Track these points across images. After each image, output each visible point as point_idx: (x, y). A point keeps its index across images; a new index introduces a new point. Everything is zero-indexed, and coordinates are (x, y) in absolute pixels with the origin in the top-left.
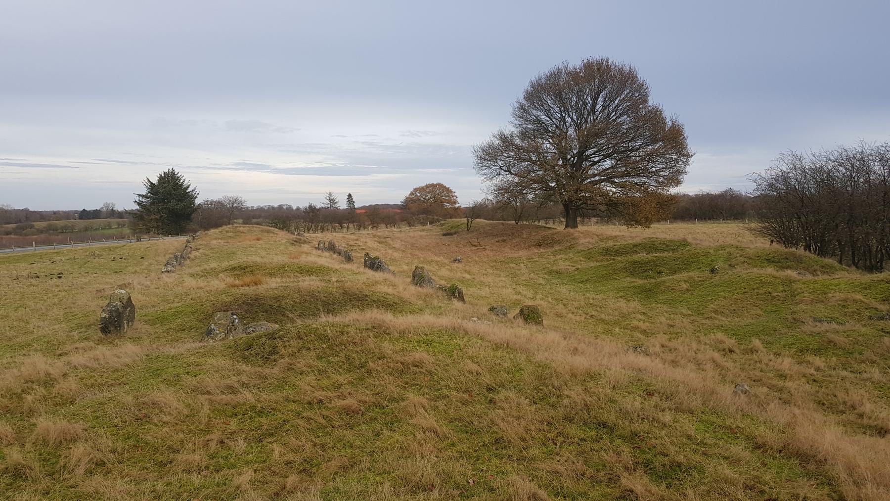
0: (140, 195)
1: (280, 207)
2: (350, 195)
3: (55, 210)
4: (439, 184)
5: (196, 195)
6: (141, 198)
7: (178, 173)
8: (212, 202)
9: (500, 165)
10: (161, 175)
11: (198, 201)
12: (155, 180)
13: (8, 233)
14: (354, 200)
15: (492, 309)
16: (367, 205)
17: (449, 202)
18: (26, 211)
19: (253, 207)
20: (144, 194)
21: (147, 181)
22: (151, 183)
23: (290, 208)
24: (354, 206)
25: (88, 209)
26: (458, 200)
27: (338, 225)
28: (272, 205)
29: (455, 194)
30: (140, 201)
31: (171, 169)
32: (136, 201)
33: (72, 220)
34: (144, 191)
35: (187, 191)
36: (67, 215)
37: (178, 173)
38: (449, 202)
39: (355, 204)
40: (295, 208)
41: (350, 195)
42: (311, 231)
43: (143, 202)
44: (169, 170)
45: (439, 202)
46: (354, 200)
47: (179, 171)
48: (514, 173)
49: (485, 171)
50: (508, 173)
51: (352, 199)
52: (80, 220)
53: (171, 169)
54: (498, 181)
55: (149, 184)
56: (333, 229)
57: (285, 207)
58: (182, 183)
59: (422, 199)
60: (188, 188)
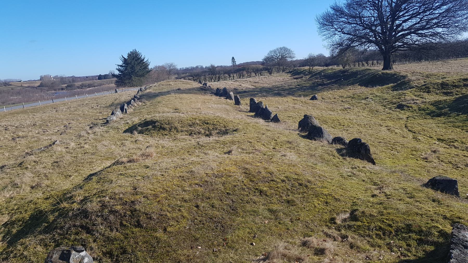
0: (118, 65)
1: (197, 67)
2: (233, 58)
3: (87, 75)
4: (284, 47)
5: (149, 63)
6: (119, 67)
7: (138, 52)
8: (159, 67)
9: (335, 28)
10: (129, 54)
11: (150, 67)
12: (126, 57)
13: (62, 89)
14: (235, 61)
15: (32, 187)
16: (242, 63)
17: (290, 57)
18: (73, 77)
19: (183, 68)
20: (121, 64)
21: (122, 57)
22: (124, 58)
23: (202, 68)
24: (236, 64)
25: (102, 74)
26: (296, 55)
27: (227, 75)
28: (193, 66)
29: (294, 52)
30: (119, 69)
31: (134, 50)
32: (117, 69)
33: (95, 81)
34: (121, 63)
35: (144, 61)
36: (93, 78)
37: (138, 52)
38: (290, 57)
39: (236, 63)
40: (204, 67)
41: (233, 58)
42: (213, 80)
43: (121, 69)
44: (133, 50)
45: (283, 58)
46: (235, 61)
47: (139, 50)
48: (346, 32)
49: (325, 33)
50: (341, 33)
51: (235, 60)
52: (99, 80)
53: (134, 50)
54: (337, 38)
55: (123, 59)
56: (225, 79)
57: (199, 67)
58: (141, 57)
59: (274, 57)
60: (143, 60)
